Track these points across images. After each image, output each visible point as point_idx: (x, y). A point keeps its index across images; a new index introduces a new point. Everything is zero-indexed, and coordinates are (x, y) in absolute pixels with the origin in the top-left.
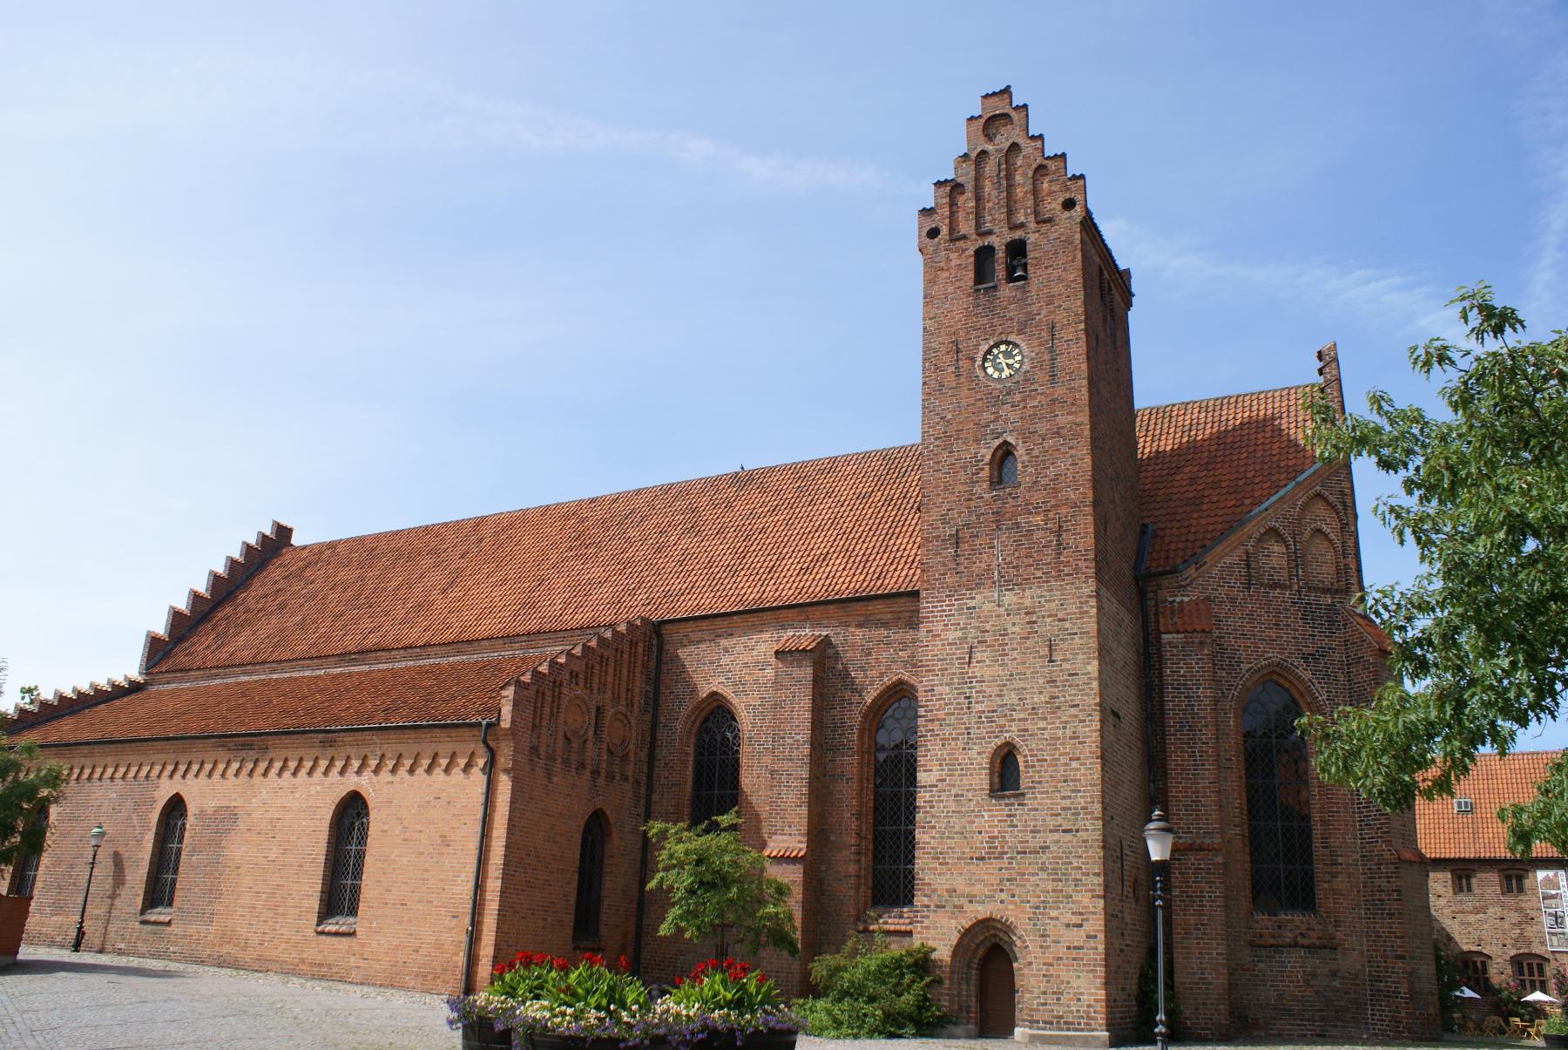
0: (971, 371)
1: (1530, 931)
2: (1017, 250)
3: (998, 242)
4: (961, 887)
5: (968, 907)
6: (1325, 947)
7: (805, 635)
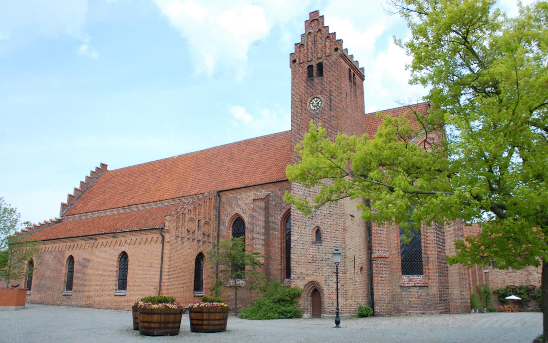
0: (306, 108)
1: (531, 277)
2: (320, 66)
3: (314, 64)
4: (304, 272)
5: (306, 278)
6: (425, 286)
7: (262, 193)
